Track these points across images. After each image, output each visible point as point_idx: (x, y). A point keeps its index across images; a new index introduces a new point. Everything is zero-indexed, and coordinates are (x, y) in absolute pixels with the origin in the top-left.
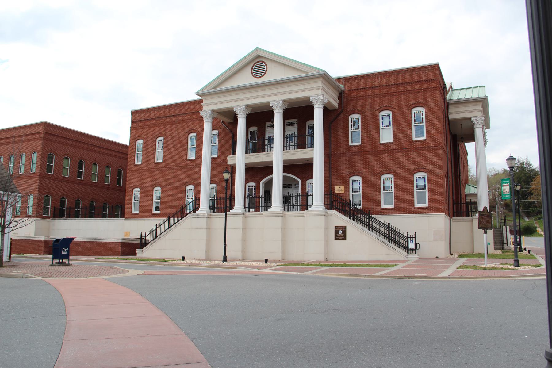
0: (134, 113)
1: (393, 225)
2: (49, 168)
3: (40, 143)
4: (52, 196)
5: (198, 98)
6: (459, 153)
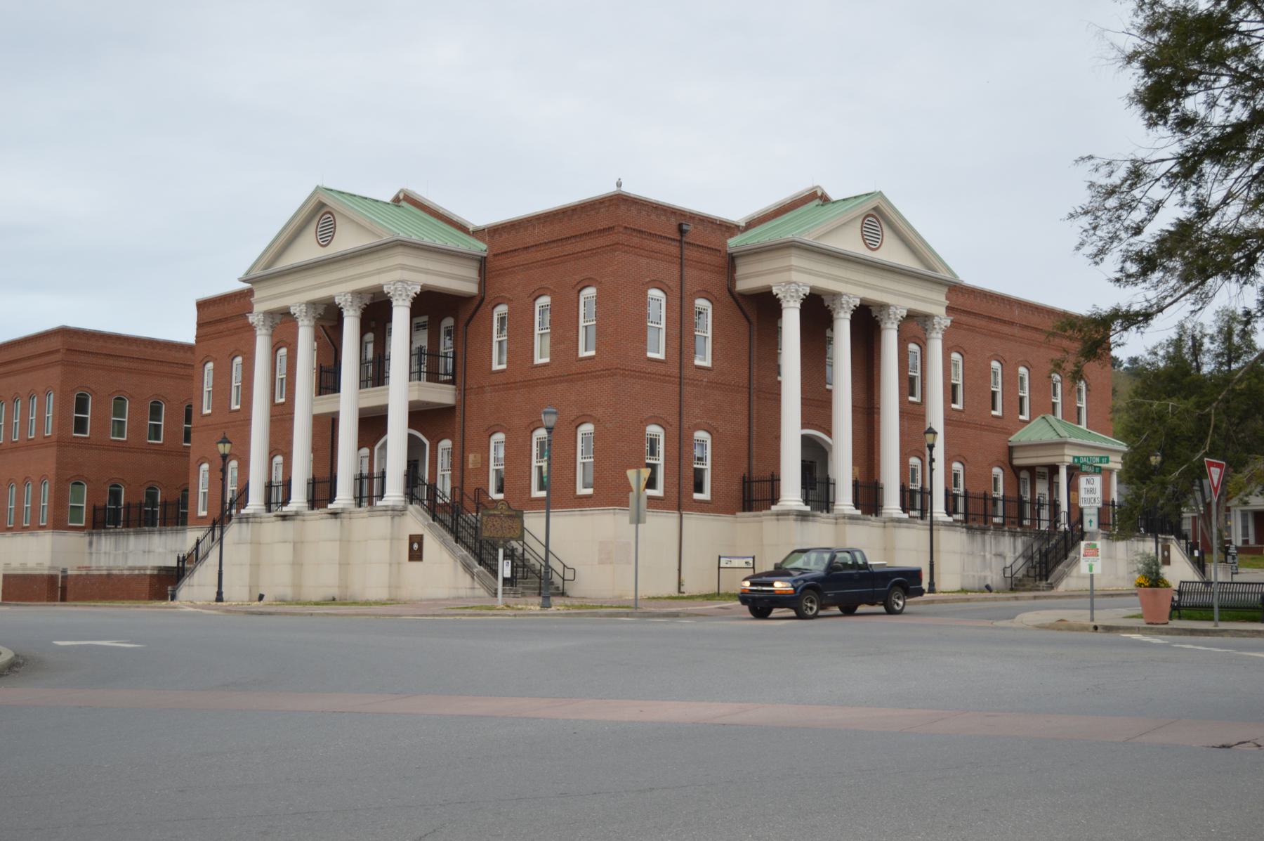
0: (202, 305)
2: (80, 425)
3: (56, 372)
4: (88, 482)
5: (247, 286)
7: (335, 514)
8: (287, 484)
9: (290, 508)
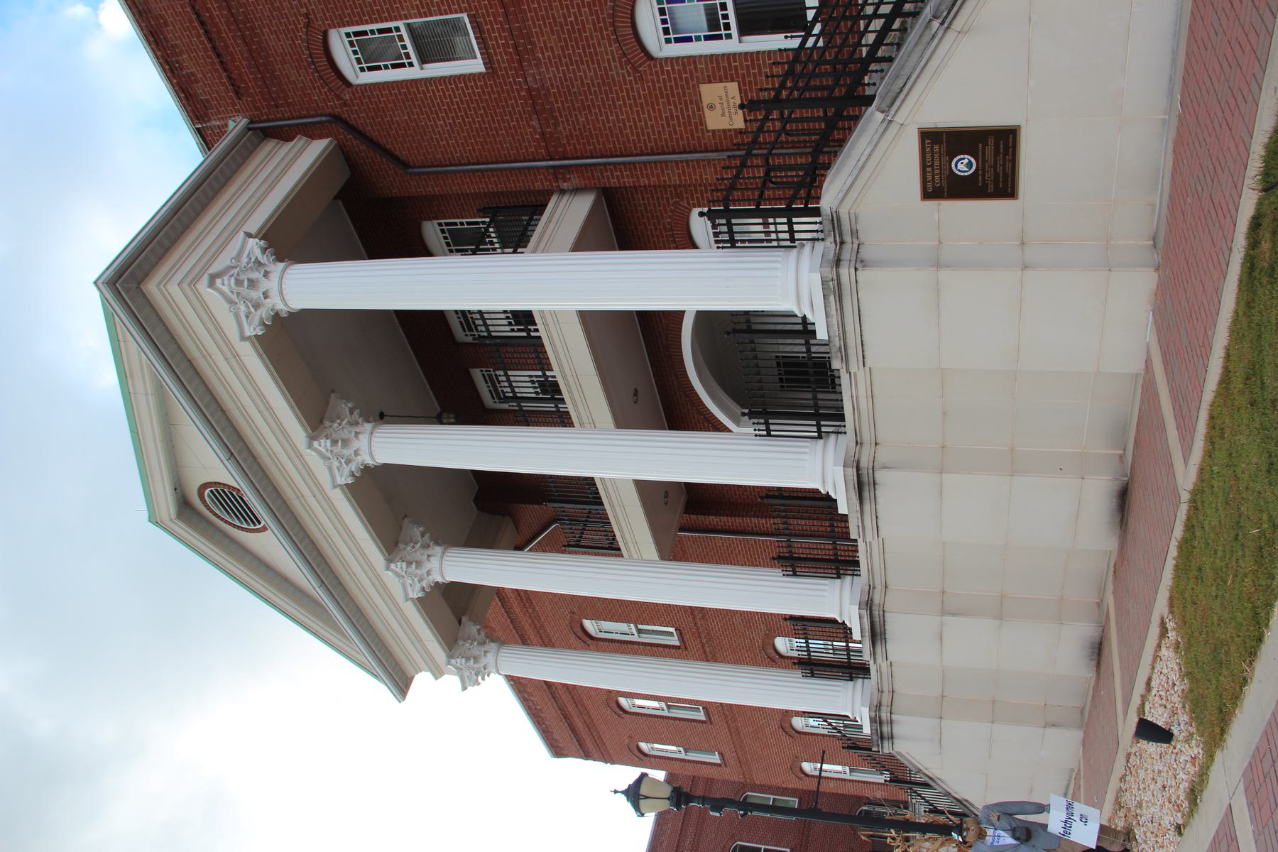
0: (436, 678)
1: (1190, 487)
6: (1267, 147)
7: (863, 485)
8: (802, 625)
9: (853, 618)
